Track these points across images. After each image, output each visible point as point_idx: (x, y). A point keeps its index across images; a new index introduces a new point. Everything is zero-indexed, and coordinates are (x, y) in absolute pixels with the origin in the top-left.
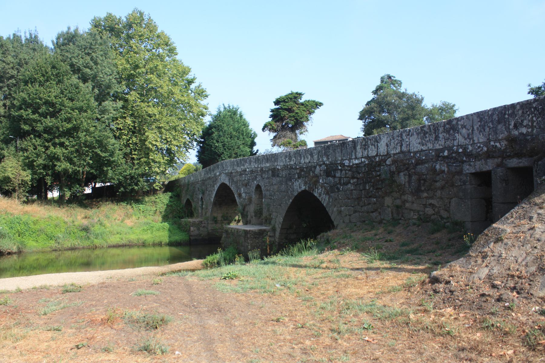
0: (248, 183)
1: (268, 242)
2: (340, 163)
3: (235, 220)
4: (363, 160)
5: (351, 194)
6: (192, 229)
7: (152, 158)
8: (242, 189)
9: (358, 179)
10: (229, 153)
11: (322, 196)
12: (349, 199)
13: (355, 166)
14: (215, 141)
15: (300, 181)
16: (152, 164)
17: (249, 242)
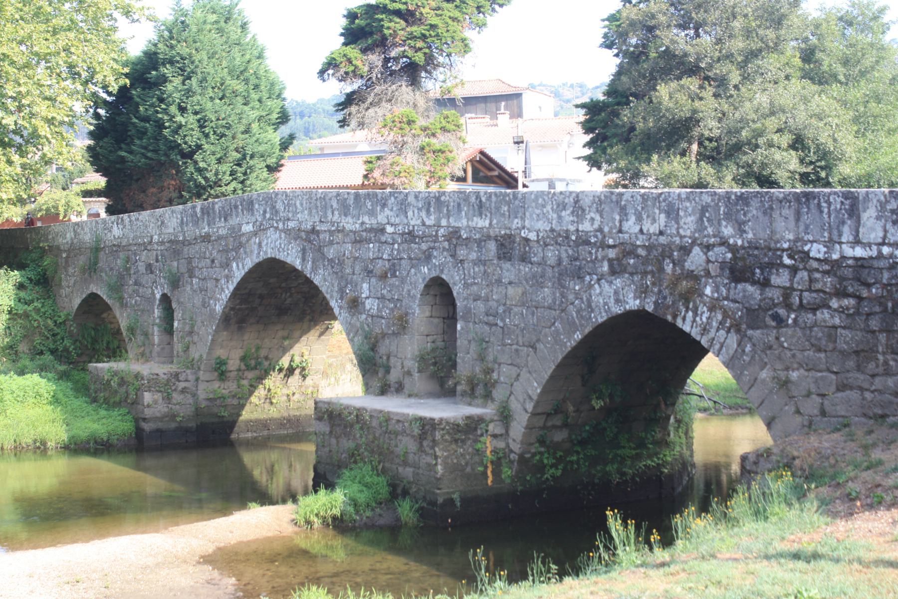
0: (393, 270)
1: (488, 452)
2: (789, 249)
5: (832, 338)
6: (148, 397)
8: (365, 286)
9: (860, 299)
12: (819, 350)
13: (850, 262)
14: (173, 109)
15: (618, 282)
17: (439, 453)
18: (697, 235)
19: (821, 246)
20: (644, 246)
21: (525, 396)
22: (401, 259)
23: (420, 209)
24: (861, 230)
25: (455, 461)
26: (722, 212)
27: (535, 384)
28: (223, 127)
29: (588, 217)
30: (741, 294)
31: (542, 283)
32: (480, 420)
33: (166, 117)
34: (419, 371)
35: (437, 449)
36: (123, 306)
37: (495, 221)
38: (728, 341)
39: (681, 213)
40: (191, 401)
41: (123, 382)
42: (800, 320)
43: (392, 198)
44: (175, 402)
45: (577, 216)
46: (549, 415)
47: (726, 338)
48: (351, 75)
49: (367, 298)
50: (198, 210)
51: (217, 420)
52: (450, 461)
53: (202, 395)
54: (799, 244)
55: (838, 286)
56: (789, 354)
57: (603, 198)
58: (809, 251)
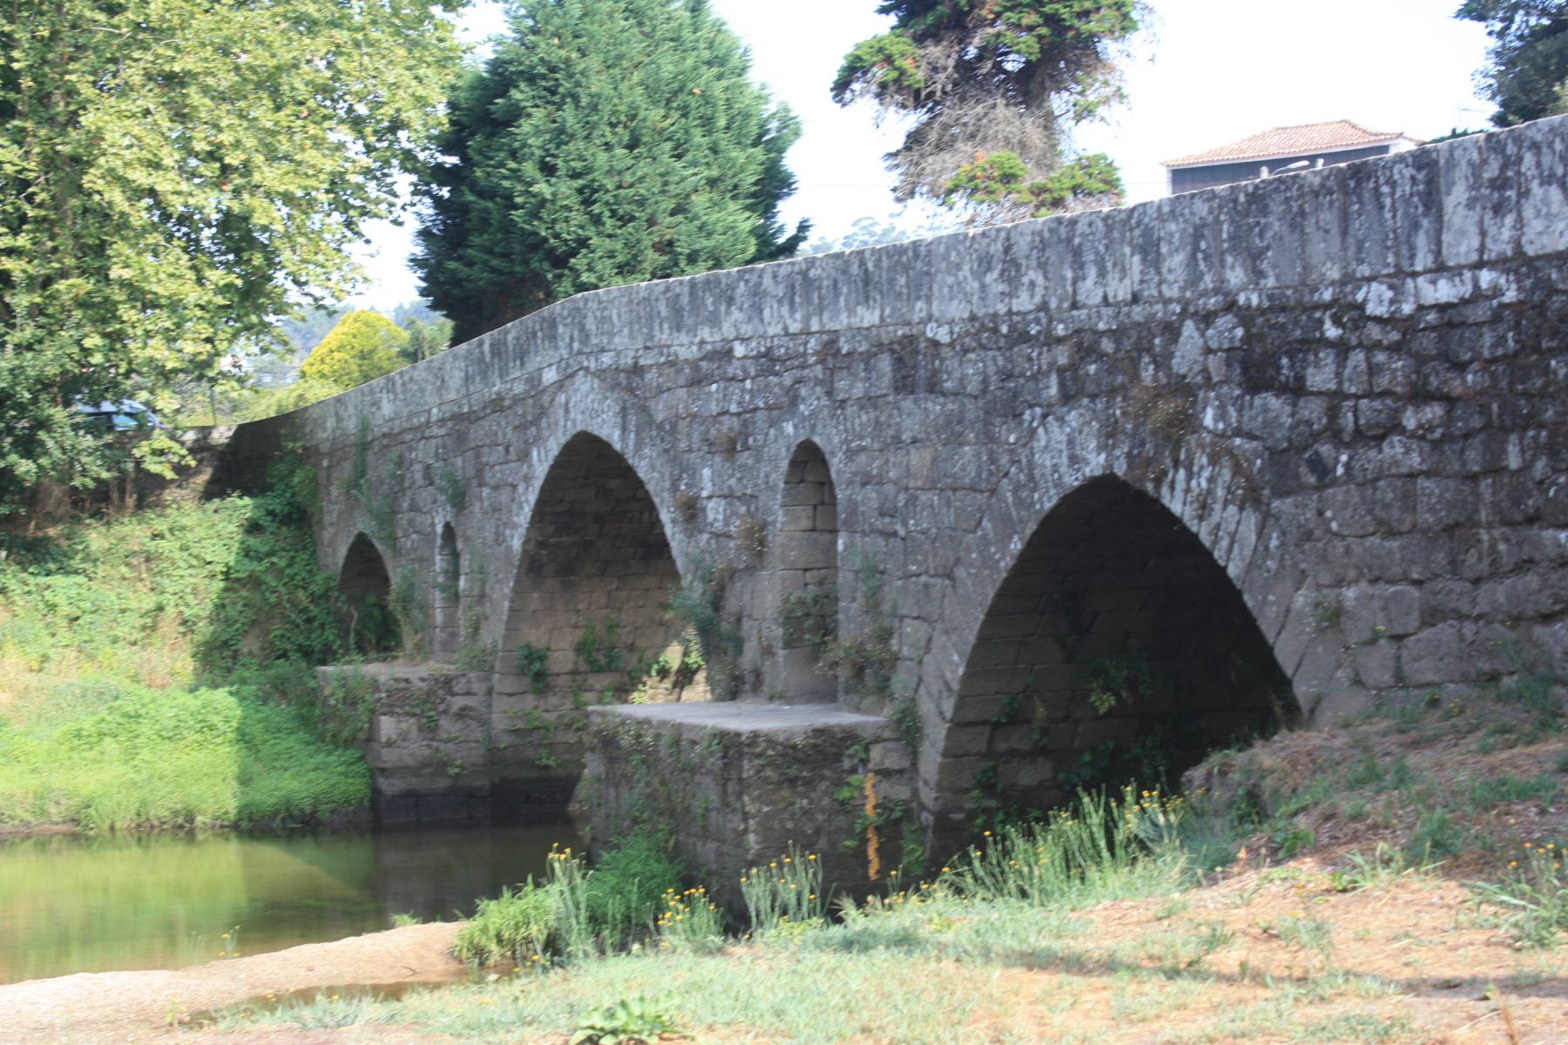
0: (744, 433)
3: (663, 673)
4: (1486, 277)
5: (1408, 501)
6: (388, 726)
7: (127, 274)
8: (706, 472)
9: (1449, 401)
10: (619, 246)
11: (1216, 517)
12: (1392, 533)
13: (1431, 317)
14: (529, 169)
15: (1073, 418)
16: (128, 313)
17: (751, 808)
18: (1188, 294)
19: (1384, 287)
20: (1110, 331)
21: (942, 687)
22: (756, 409)
23: (780, 301)
24: (1445, 238)
25: (790, 825)
26: (1225, 236)
27: (956, 658)
28: (631, 202)
29: (1025, 280)
30: (1260, 419)
31: (961, 434)
32: (849, 737)
33: (519, 187)
34: (788, 645)
35: (746, 798)
36: (397, 552)
37: (888, 312)
38: (1242, 528)
39: (1164, 249)
40: (479, 735)
41: (351, 701)
42: (1357, 465)
43: (742, 284)
44: (445, 736)
45: (1010, 281)
46: (996, 726)
47: (1238, 523)
48: (892, 88)
49: (710, 498)
50: (486, 348)
51: (534, 774)
52: (776, 825)
53: (499, 723)
54: (1348, 289)
55: (1414, 377)
56: (1340, 546)
57: (1046, 234)
58: (1365, 300)
